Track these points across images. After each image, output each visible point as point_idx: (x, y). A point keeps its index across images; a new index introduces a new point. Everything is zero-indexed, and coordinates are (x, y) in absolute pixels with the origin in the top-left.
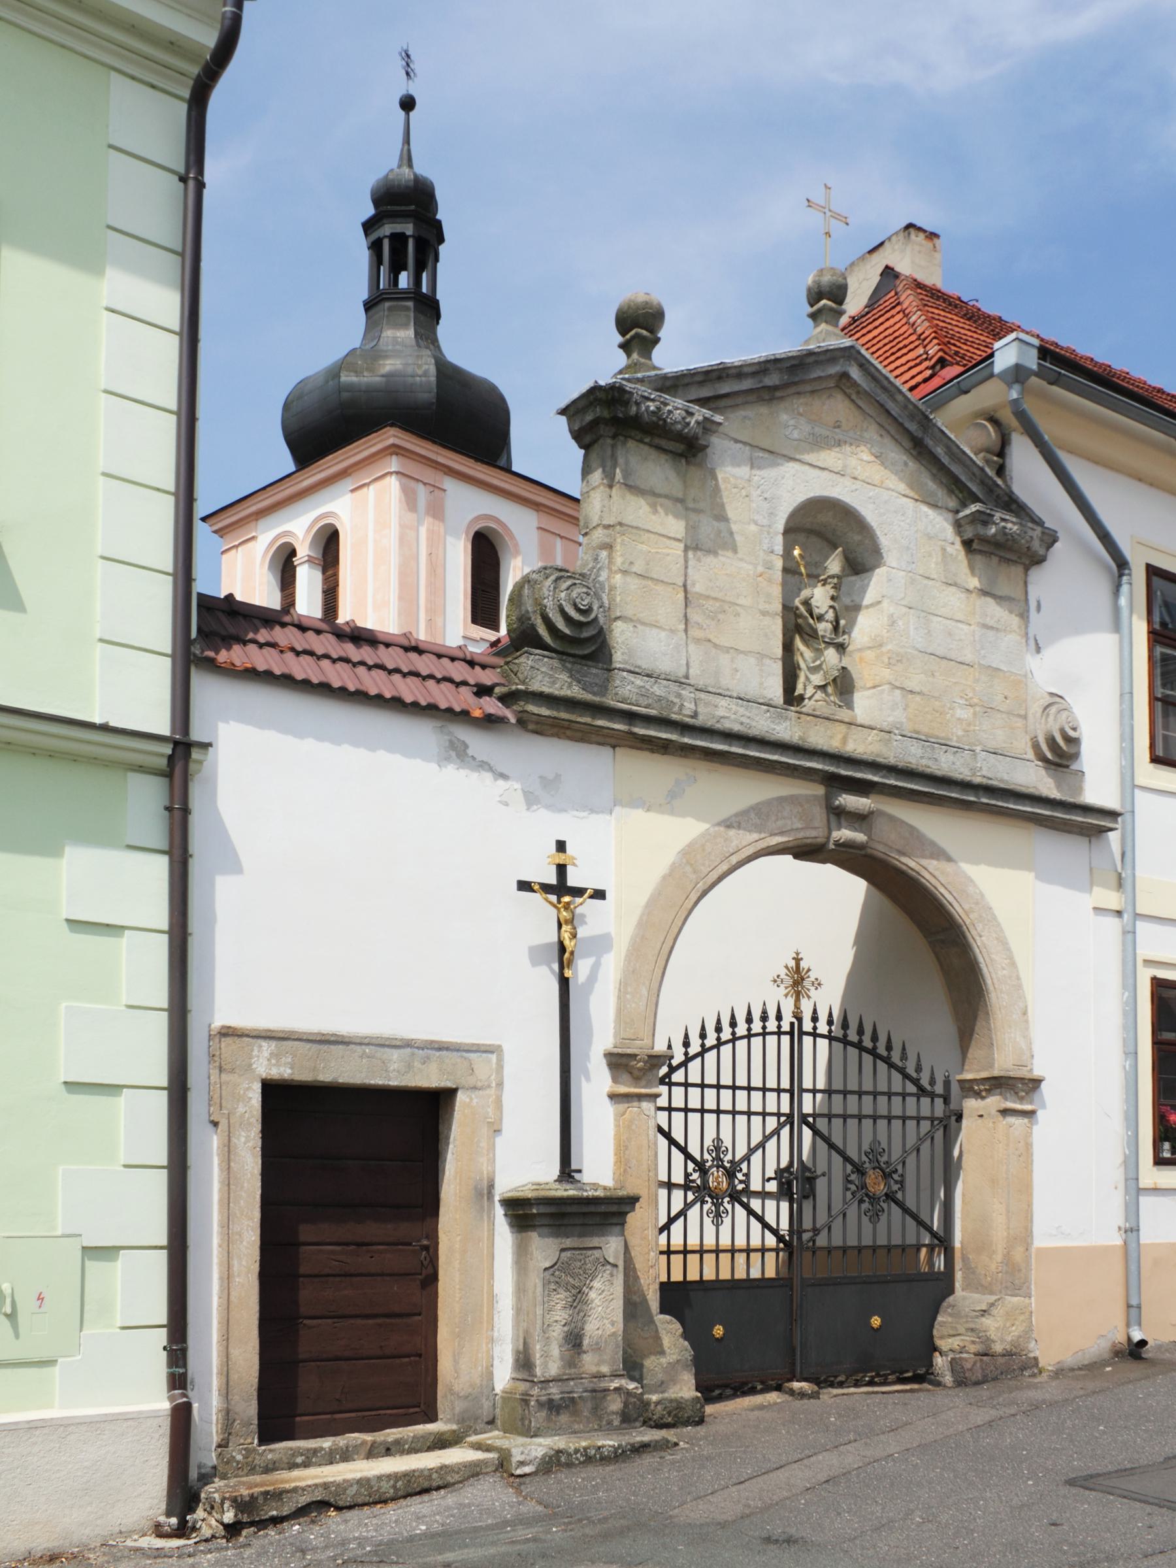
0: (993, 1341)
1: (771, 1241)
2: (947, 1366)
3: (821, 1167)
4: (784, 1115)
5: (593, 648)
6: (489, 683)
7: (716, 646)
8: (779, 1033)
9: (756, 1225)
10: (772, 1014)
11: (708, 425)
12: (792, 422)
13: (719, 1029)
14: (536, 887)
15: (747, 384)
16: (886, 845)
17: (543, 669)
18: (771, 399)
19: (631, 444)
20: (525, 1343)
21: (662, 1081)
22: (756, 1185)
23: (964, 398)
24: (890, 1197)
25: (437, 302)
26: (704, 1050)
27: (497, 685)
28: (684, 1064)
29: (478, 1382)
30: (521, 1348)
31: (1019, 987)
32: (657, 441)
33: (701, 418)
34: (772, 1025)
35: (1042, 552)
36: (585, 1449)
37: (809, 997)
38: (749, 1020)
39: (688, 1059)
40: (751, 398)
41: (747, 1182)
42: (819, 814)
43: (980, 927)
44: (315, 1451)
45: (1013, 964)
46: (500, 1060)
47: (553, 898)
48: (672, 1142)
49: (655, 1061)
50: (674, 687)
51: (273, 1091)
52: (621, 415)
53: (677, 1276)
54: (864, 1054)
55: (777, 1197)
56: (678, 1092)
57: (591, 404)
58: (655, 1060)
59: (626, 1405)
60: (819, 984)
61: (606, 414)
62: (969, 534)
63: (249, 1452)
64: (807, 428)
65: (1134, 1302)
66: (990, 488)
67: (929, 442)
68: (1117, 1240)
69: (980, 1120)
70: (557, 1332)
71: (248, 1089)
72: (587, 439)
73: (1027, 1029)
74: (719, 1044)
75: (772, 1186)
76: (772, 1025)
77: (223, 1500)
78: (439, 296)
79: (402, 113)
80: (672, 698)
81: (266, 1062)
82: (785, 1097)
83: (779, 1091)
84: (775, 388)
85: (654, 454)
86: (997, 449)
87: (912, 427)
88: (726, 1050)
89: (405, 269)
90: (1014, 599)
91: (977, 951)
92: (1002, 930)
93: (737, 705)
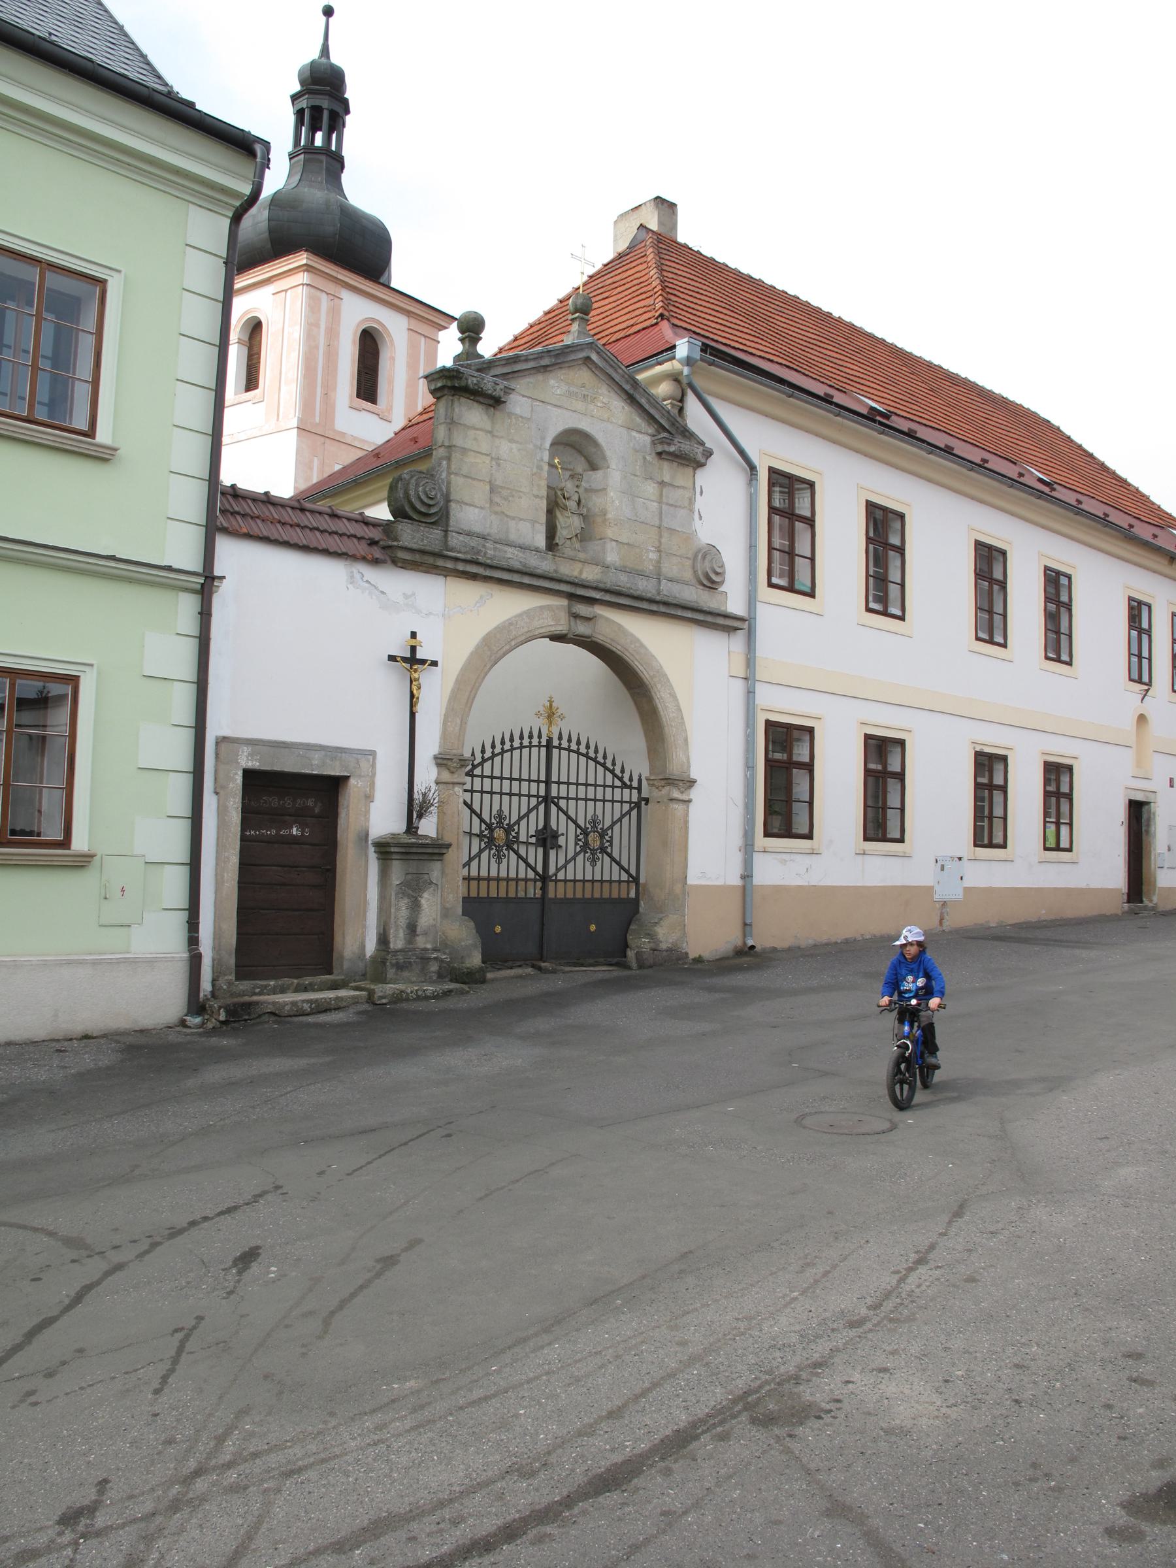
0: (661, 942)
1: (531, 875)
2: (633, 956)
3: (562, 830)
4: (541, 797)
5: (436, 518)
6: (377, 539)
7: (507, 516)
8: (539, 746)
9: (522, 865)
10: (535, 734)
11: (507, 390)
12: (556, 385)
13: (503, 743)
14: (399, 659)
15: (531, 365)
16: (603, 635)
17: (408, 531)
18: (546, 371)
19: (463, 400)
20: (384, 929)
21: (467, 774)
22: (523, 838)
23: (659, 366)
24: (603, 850)
25: (342, 158)
26: (494, 755)
27: (382, 540)
28: (481, 764)
29: (357, 951)
30: (382, 931)
31: (683, 723)
32: (478, 398)
33: (502, 387)
34: (535, 741)
35: (703, 461)
36: (417, 991)
37: (557, 725)
38: (521, 738)
39: (484, 760)
40: (532, 372)
41: (517, 837)
42: (563, 617)
43: (659, 686)
44: (266, 986)
45: (680, 710)
46: (374, 759)
47: (408, 666)
48: (473, 811)
49: (463, 763)
50: (481, 541)
51: (248, 774)
52: (457, 385)
53: (474, 894)
54: (589, 761)
55: (536, 845)
56: (477, 781)
57: (441, 377)
58: (463, 762)
59: (440, 967)
60: (564, 717)
61: (449, 384)
62: (660, 448)
63: (230, 984)
64: (565, 388)
65: (748, 921)
66: (673, 423)
67: (638, 397)
68: (737, 882)
69: (658, 805)
70: (403, 922)
71: (236, 774)
72: (438, 395)
73: (688, 749)
74: (503, 752)
75: (533, 840)
76: (535, 741)
77: (220, 1008)
78: (344, 153)
79: (324, 18)
80: (480, 548)
81: (245, 759)
82: (542, 786)
83: (538, 782)
84: (547, 366)
85: (475, 404)
86: (679, 397)
87: (627, 387)
88: (507, 756)
89: (320, 130)
90: (686, 488)
91: (657, 701)
92: (673, 689)
93: (518, 551)
